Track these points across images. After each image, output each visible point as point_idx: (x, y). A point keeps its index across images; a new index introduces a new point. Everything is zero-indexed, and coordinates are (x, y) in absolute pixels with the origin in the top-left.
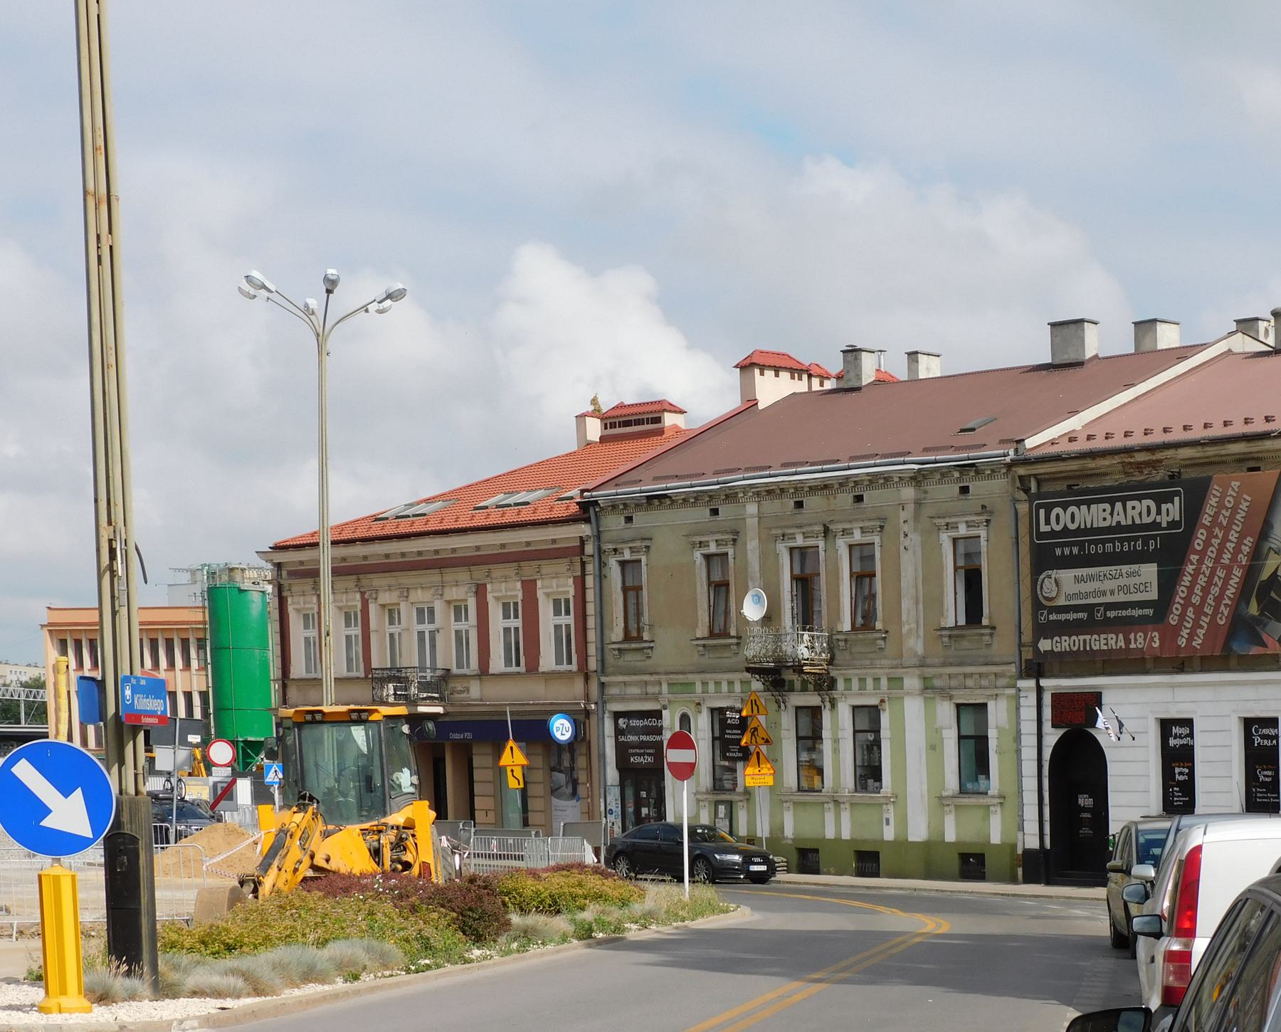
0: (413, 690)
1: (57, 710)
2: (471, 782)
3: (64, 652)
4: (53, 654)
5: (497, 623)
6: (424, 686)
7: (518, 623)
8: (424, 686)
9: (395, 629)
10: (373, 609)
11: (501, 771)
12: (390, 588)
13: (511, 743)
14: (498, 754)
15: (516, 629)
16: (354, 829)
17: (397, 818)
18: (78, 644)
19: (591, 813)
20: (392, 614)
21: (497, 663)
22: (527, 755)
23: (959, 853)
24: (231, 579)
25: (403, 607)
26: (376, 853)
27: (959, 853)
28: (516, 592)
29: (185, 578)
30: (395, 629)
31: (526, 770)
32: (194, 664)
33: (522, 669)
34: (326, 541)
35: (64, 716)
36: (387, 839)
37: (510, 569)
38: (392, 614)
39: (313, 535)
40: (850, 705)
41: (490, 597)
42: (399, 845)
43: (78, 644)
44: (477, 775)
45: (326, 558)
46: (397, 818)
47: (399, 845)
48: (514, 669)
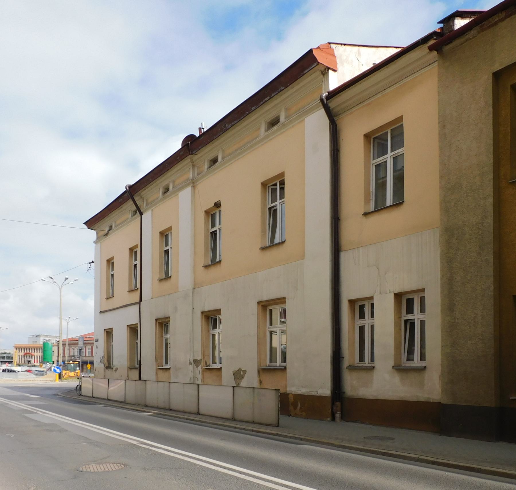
0: (76, 358)
1: (15, 358)
2: (83, 368)
3: (17, 350)
4: (15, 350)
5: (88, 351)
6: (77, 358)
7: (90, 351)
8: (77, 358)
9: (74, 351)
10: (71, 349)
11: (87, 367)
12: (73, 346)
13: (89, 364)
14: (87, 365)
15: (90, 352)
16: (73, 372)
17: (77, 372)
18: (19, 349)
19: (196, 418)
20: (74, 349)
21: (87, 355)
22: (91, 365)
23: (348, 300)
24: (47, 342)
25: (75, 348)
26: (75, 374)
27: (348, 300)
28: (90, 347)
29: (32, 336)
30: (74, 351)
31: (90, 367)
32: (38, 352)
33: (91, 356)
34: (67, 340)
35: (16, 359)
36: (76, 373)
37: (90, 345)
38: (74, 349)
39: (65, 339)
40: (115, 373)
41: (87, 348)
42: (77, 374)
43: (19, 349)
44: (84, 368)
45: (67, 343)
46: (77, 372)
47: (77, 374)
48: (89, 356)
